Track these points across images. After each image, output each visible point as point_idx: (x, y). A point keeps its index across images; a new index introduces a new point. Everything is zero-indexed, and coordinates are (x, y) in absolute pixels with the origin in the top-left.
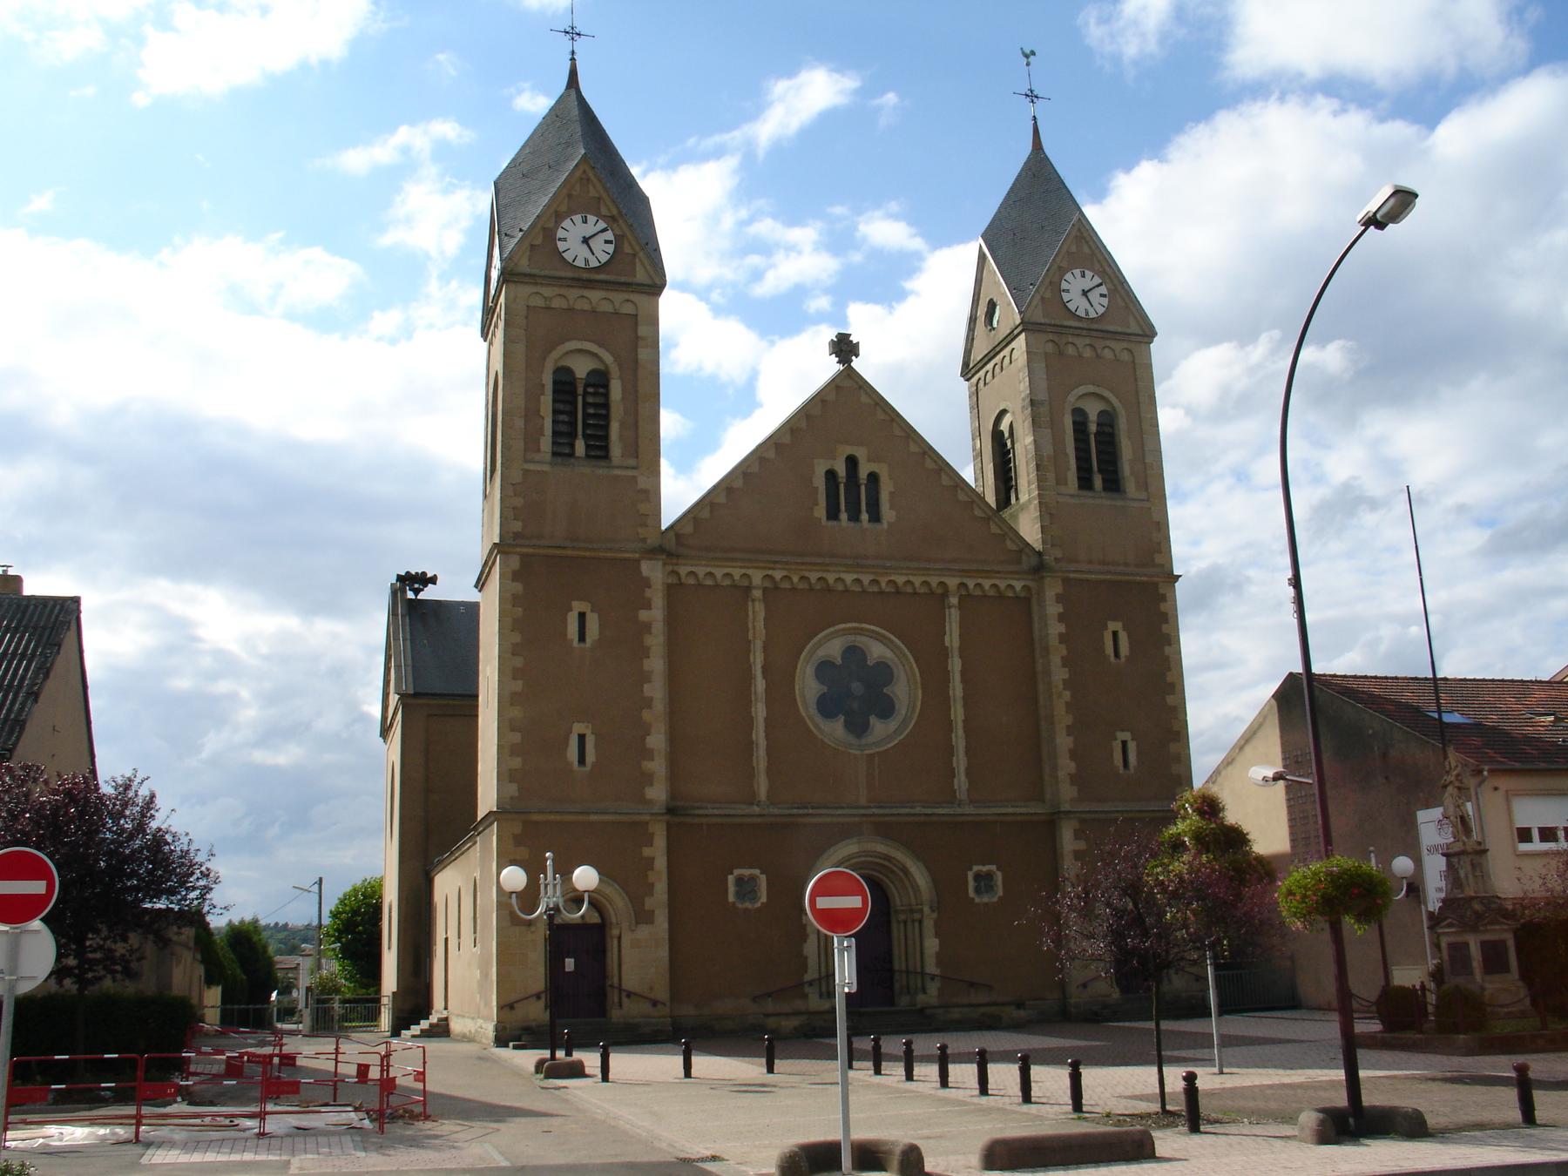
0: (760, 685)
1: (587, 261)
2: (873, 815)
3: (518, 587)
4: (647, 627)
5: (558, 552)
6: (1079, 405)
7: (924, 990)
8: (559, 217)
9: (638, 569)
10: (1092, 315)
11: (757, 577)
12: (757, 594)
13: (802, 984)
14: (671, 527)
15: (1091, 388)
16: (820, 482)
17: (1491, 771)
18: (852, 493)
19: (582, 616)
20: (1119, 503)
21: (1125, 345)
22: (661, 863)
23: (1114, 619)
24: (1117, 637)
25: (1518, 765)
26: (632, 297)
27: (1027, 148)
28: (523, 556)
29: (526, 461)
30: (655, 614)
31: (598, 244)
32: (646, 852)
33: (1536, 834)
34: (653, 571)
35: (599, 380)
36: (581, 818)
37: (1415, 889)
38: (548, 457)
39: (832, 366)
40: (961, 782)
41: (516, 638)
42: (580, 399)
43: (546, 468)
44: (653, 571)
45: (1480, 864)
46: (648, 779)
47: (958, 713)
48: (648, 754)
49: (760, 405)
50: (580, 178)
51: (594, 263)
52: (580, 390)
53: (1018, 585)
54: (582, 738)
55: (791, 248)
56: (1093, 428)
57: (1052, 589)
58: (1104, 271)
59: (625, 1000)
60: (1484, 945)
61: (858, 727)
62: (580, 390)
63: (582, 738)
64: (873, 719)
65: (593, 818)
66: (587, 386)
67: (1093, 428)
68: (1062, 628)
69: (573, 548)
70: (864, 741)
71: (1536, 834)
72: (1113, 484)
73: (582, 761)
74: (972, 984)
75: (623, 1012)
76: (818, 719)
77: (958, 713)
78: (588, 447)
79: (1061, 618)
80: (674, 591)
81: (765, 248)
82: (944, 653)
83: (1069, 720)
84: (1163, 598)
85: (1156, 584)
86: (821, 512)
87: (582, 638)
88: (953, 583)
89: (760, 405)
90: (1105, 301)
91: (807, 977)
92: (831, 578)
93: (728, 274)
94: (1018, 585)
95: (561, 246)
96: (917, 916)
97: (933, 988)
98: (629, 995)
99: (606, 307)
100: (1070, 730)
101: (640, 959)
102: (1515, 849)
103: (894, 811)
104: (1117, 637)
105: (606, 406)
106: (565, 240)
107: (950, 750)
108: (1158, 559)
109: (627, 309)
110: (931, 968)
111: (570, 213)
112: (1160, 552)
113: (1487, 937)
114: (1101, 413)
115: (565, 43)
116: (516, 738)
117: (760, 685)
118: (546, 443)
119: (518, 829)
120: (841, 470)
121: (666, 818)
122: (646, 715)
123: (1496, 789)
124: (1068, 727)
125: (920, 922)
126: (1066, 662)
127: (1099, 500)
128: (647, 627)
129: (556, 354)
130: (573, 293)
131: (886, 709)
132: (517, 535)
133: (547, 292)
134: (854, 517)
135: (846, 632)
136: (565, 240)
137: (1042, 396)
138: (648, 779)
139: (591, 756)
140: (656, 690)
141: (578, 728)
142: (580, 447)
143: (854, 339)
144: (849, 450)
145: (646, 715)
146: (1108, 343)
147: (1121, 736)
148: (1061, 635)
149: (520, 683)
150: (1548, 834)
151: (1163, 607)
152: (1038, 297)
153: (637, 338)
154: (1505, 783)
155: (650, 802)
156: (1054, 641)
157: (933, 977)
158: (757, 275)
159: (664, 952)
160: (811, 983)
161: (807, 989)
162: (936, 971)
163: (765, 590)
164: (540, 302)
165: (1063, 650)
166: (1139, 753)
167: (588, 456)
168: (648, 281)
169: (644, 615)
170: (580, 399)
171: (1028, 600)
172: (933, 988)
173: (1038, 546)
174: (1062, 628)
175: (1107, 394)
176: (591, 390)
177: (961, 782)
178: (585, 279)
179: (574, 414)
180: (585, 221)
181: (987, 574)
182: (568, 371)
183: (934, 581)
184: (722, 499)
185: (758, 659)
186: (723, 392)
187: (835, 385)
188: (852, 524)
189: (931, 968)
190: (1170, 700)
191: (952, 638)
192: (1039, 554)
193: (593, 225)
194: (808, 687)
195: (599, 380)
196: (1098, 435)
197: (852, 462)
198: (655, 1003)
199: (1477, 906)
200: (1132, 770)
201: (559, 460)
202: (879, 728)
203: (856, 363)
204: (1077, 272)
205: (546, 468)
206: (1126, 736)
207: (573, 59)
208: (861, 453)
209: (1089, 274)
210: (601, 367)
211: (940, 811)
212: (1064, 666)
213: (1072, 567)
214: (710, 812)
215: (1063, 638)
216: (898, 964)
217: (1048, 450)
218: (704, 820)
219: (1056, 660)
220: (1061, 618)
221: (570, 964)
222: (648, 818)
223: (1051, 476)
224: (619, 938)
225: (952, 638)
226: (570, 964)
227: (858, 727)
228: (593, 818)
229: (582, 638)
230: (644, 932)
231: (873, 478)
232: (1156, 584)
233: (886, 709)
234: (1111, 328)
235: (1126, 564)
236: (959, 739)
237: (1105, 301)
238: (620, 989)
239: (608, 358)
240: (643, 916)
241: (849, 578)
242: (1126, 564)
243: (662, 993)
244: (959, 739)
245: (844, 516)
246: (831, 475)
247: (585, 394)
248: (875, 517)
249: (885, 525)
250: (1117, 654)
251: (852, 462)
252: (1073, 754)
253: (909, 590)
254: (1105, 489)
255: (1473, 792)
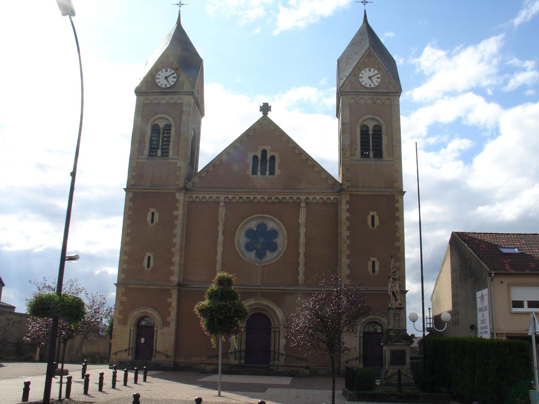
0: (221, 238)
1: (166, 85)
2: (261, 289)
3: (131, 204)
4: (176, 217)
5: (145, 191)
6: (365, 123)
7: (278, 359)
8: (360, 70)
9: (175, 196)
10: (373, 86)
11: (222, 198)
12: (222, 204)
13: (228, 353)
14: (343, 180)
15: (370, 116)
16: (250, 161)
17: (495, 274)
18: (264, 162)
19: (153, 213)
20: (379, 162)
21: (387, 97)
22: (174, 304)
23: (372, 211)
24: (373, 216)
25: (532, 272)
26: (181, 96)
27: (174, 25)
28: (134, 193)
29: (138, 159)
30: (180, 213)
31: (374, 79)
32: (169, 300)
33: (526, 304)
34: (180, 196)
35: (168, 128)
36: (146, 287)
37: (297, 325)
38: (146, 157)
39: (261, 115)
40: (301, 277)
41: (129, 222)
42: (161, 135)
43: (145, 161)
44: (180, 196)
45: (399, 315)
46: (172, 273)
47: (302, 250)
48: (173, 264)
49: (501, 134)
50: (368, 55)
51: (168, 86)
52: (161, 132)
53: (332, 198)
54: (149, 258)
55: (524, 70)
56: (371, 132)
57: (345, 199)
58: (380, 68)
59: (157, 354)
60: (393, 352)
61: (261, 255)
62: (161, 132)
63: (149, 258)
64: (268, 252)
65: (150, 287)
66: (164, 130)
67: (371, 132)
68: (348, 215)
69: (151, 189)
70: (262, 260)
71: (526, 304)
72: (378, 154)
73: (148, 266)
74: (299, 358)
75: (157, 358)
76: (245, 251)
77: (302, 250)
78: (374, 154)
79: (348, 211)
80: (190, 205)
81: (513, 70)
82: (298, 226)
83: (348, 252)
84: (397, 201)
85: (394, 196)
86: (250, 172)
87: (152, 222)
88: (303, 197)
89: (501, 134)
90: (379, 80)
91: (230, 351)
92: (252, 197)
93: (495, 82)
94: (332, 198)
95: (361, 80)
96: (278, 330)
97: (282, 359)
98: (158, 352)
99: (172, 101)
100: (348, 257)
101: (164, 340)
102: (510, 310)
103: (270, 288)
104: (373, 216)
105: (169, 137)
106: (362, 78)
107: (298, 264)
108: (396, 185)
109: (180, 101)
110: (282, 351)
111: (364, 68)
112: (397, 182)
113: (394, 348)
114: (375, 126)
115: (177, 8)
116: (126, 257)
117: (221, 238)
118: (146, 151)
119: (124, 290)
120: (259, 155)
121: (177, 288)
122: (173, 250)
123: (502, 282)
124: (348, 255)
125: (279, 332)
126: (349, 229)
127: (372, 162)
128: (176, 217)
129: (152, 120)
130: (162, 97)
131: (273, 248)
132: (132, 185)
133: (151, 98)
134: (263, 173)
135: (258, 218)
136: (362, 78)
137: (347, 121)
138: (172, 273)
139: (152, 265)
140: (177, 240)
141: (148, 254)
142: (159, 152)
143: (262, 105)
144: (264, 147)
145: (173, 250)
146: (379, 97)
147: (372, 259)
148: (347, 218)
149: (129, 238)
150: (531, 304)
151: (397, 205)
152: (348, 81)
153: (182, 111)
154: (507, 280)
155: (172, 282)
156: (344, 220)
157: (282, 354)
158: (506, 83)
159: (173, 338)
160: (231, 353)
161: (229, 355)
162: (284, 352)
163: (225, 202)
164: (148, 102)
165: (348, 224)
166: (380, 266)
167: (162, 156)
168: (394, 91)
169: (175, 213)
170: (161, 135)
171: (337, 204)
172: (282, 359)
173: (341, 182)
174: (348, 215)
175: (377, 118)
176: (166, 132)
177: (301, 277)
178: (165, 92)
179: (158, 141)
180: (370, 71)
181: (309, 193)
182: (157, 125)
183: (295, 197)
184: (211, 169)
185: (220, 229)
186: (220, 127)
187: (259, 122)
188: (262, 176)
189: (282, 351)
190: (397, 244)
191: (302, 219)
192: (341, 184)
193: (373, 72)
194: (241, 239)
195: (168, 128)
196: (372, 133)
197: (264, 152)
198: (168, 356)
199: (392, 333)
200: (376, 273)
201: (150, 158)
202: (270, 256)
203: (270, 115)
204: (164, 70)
205: (145, 161)
206: (375, 259)
207: (179, 14)
208: (268, 148)
209: (372, 70)
210: (378, 124)
211: (291, 288)
212: (348, 230)
213: (354, 189)
214: (197, 286)
215: (348, 219)
216: (272, 349)
217: (348, 142)
218: (193, 289)
219: (344, 228)
220: (348, 211)
221: (143, 340)
222: (170, 288)
223: (348, 153)
224: (157, 331)
225: (302, 219)
226: (143, 340)
227: (261, 255)
228: (150, 287)
229: (152, 222)
230: (165, 330)
231: (273, 158)
232: (394, 196)
233: (273, 248)
234: (381, 91)
235: (380, 188)
236: (302, 260)
237: (379, 80)
238: (156, 351)
239: (171, 120)
240: (166, 324)
241: (259, 197)
242: (380, 188)
243: (171, 353)
244: (302, 260)
245: (259, 173)
246: (255, 157)
247: (164, 133)
248: (272, 173)
249: (276, 175)
250: (373, 225)
251: (264, 152)
252: (349, 267)
253: (285, 201)
254: (374, 157)
255: (489, 284)
